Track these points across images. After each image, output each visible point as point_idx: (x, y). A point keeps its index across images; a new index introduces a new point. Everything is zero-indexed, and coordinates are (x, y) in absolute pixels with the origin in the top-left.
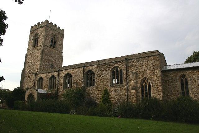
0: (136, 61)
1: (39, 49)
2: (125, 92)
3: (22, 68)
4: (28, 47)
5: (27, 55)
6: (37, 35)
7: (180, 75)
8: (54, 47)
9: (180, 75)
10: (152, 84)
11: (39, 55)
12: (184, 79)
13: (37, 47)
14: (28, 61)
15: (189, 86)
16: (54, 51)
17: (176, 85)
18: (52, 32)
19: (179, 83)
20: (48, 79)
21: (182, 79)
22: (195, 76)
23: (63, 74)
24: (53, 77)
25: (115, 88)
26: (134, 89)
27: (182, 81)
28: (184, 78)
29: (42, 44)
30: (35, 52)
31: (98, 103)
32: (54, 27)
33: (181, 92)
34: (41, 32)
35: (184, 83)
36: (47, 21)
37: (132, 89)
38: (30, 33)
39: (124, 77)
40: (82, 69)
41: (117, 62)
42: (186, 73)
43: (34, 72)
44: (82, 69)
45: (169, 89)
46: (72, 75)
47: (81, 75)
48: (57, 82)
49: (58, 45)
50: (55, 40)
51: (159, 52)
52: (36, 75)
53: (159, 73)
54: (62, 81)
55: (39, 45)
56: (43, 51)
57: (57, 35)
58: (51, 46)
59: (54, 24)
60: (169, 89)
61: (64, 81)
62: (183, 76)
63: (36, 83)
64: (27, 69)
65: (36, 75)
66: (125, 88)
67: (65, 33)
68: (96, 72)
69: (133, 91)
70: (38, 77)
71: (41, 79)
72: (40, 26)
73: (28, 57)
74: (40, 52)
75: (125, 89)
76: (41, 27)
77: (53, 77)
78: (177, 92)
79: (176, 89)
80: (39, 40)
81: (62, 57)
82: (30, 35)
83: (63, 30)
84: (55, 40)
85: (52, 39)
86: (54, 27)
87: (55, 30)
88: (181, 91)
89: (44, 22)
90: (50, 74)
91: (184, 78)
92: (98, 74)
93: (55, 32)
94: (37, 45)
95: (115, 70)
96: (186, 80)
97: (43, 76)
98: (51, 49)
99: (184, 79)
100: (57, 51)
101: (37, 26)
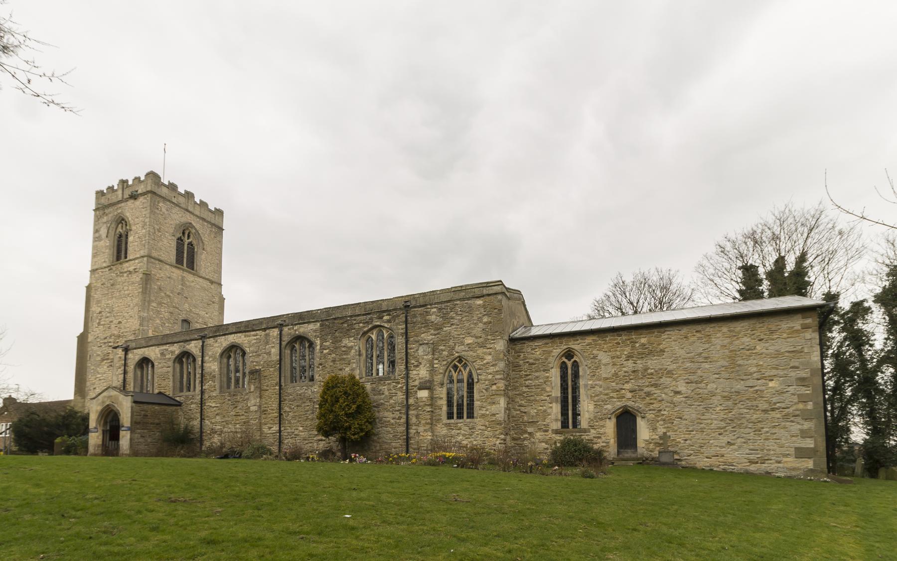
0: (435, 310)
1: (135, 271)
2: (401, 396)
3: (81, 330)
4: (92, 265)
5: (89, 288)
6: (121, 220)
7: (557, 350)
8: (191, 265)
9: (557, 350)
10: (478, 375)
11: (136, 290)
12: (569, 364)
13: (127, 264)
14: (95, 308)
15: (582, 382)
16: (190, 277)
17: (547, 380)
18: (178, 217)
19: (555, 375)
20: (170, 363)
21: (564, 363)
22: (601, 353)
23: (218, 345)
24: (184, 357)
25: (374, 385)
26: (426, 389)
27: (563, 368)
28: (569, 360)
29: (142, 253)
30: (119, 279)
31: (880, 381)
32: (182, 200)
33: (557, 397)
34: (136, 212)
35: (570, 371)
36: (153, 176)
37: (420, 389)
38: (96, 216)
39: (399, 355)
40: (275, 332)
41: (381, 313)
42: (576, 345)
43: (121, 342)
44: (275, 332)
45: (525, 389)
46: (247, 350)
47: (273, 350)
48: (199, 371)
49: (203, 260)
50: (190, 244)
51: (503, 284)
52: (126, 350)
53: (500, 345)
54: (213, 366)
55: (131, 258)
56: (147, 278)
57: (198, 226)
58: (179, 260)
59: (181, 190)
60: (525, 389)
61: (221, 368)
62: (569, 354)
63: (130, 376)
64: (96, 332)
65: (126, 350)
66: (400, 386)
67: (227, 224)
68: (318, 342)
69: (424, 394)
70: (135, 356)
71: (145, 362)
72: (127, 193)
73: (96, 295)
74: (137, 278)
75: (402, 388)
76: (134, 197)
77: (184, 357)
78: (548, 396)
79: (544, 390)
80: (131, 239)
81: (222, 300)
82: (97, 219)
83: (219, 213)
84: (190, 244)
85: (180, 239)
86: (182, 200)
87: (187, 210)
88: (559, 395)
89: (142, 178)
90: (176, 349)
91: (569, 360)
92: (322, 348)
93: (188, 218)
94: (126, 257)
95: (374, 337)
96: (576, 365)
97: (153, 353)
98: (177, 273)
99: (569, 364)
100: (201, 280)
101: (120, 192)
